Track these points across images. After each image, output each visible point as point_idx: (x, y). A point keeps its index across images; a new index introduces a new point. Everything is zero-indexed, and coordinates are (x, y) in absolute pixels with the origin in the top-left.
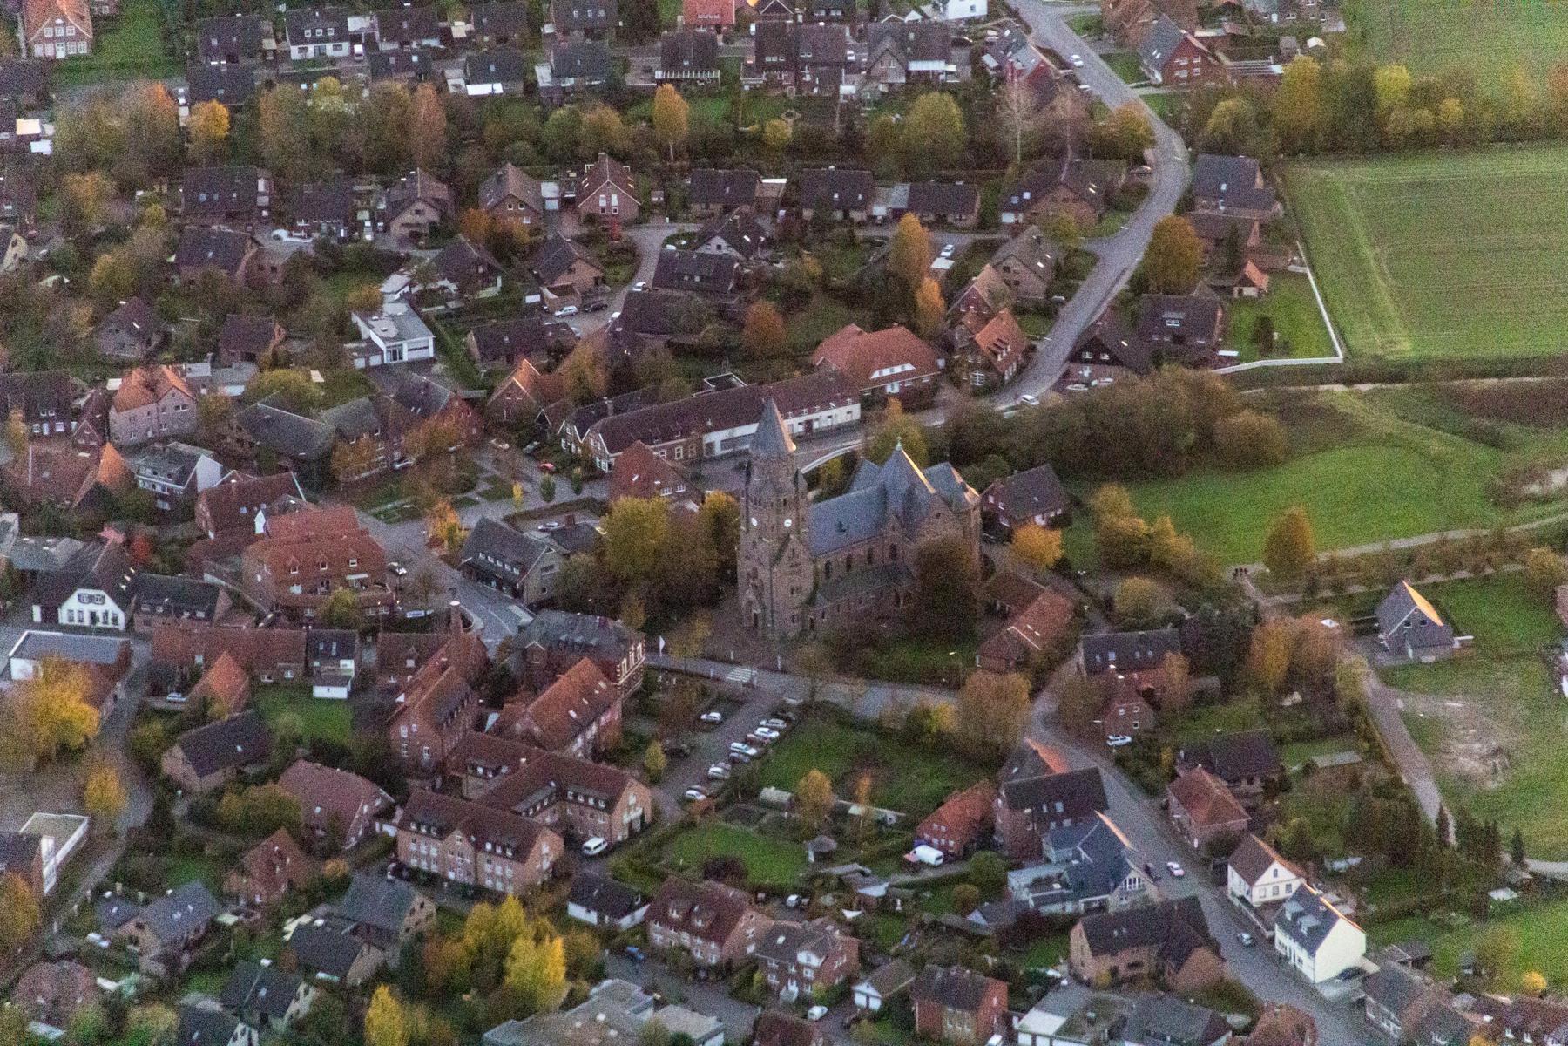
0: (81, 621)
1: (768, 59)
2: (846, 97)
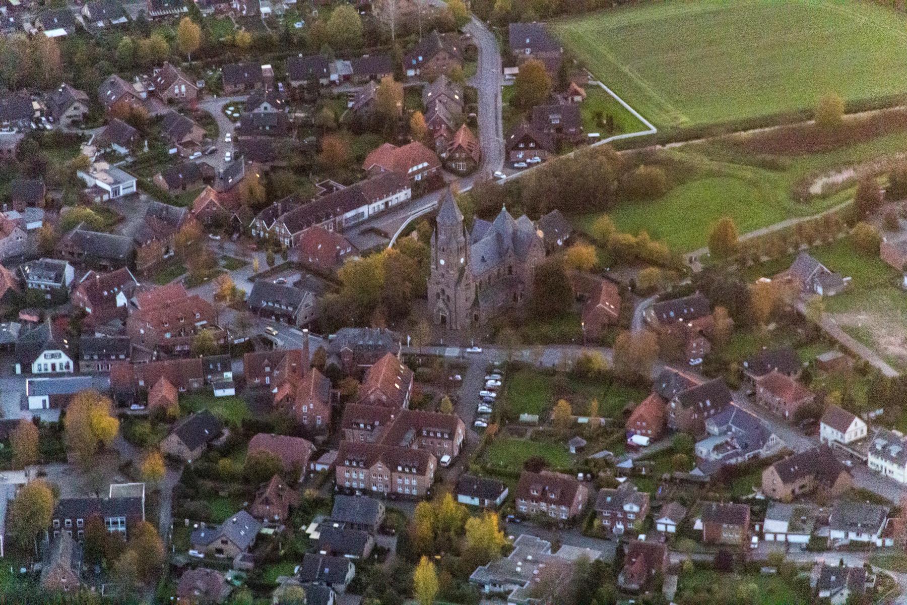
0: (46, 370)
2: (266, 14)
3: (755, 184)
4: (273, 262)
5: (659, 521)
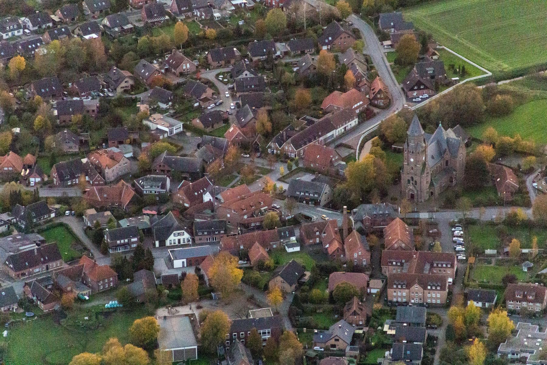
0: (175, 243)
1: (182, 9)
2: (218, 18)
4: (291, 168)
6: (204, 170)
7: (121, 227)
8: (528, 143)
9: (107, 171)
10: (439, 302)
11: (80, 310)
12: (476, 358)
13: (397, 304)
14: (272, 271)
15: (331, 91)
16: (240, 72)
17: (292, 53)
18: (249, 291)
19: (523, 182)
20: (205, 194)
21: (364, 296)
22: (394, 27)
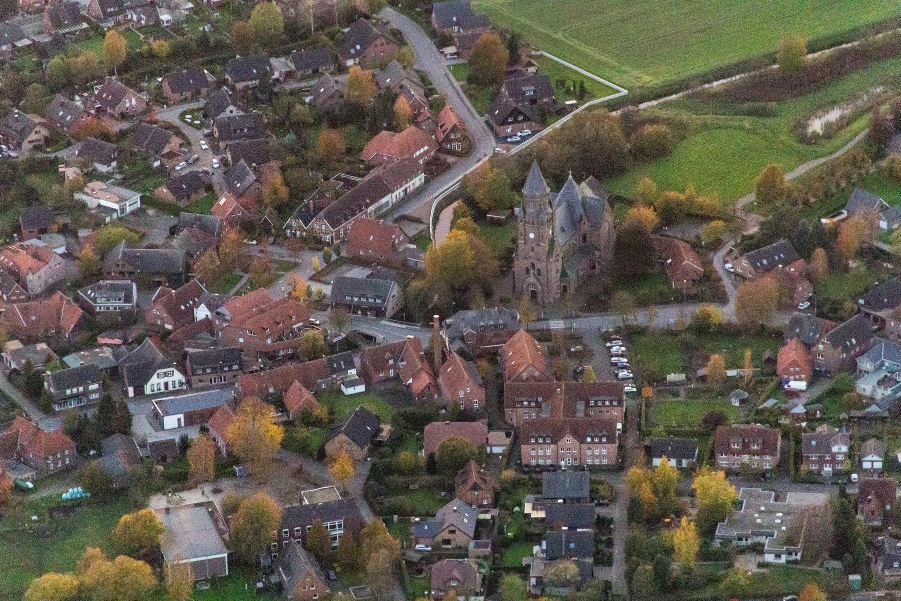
0: (159, 390)
1: (109, 10)
2: (167, 22)
3: (753, 132)
5: (864, 459)
6: (188, 268)
7: (69, 367)
8: (707, 200)
9: (30, 277)
10: (605, 462)
11: (22, 504)
12: (684, 550)
13: (538, 470)
14: (330, 426)
15: (375, 132)
16: (221, 108)
17: (299, 74)
18: (295, 461)
19: (707, 264)
20: (197, 307)
21: (485, 459)
22: (457, 24)
